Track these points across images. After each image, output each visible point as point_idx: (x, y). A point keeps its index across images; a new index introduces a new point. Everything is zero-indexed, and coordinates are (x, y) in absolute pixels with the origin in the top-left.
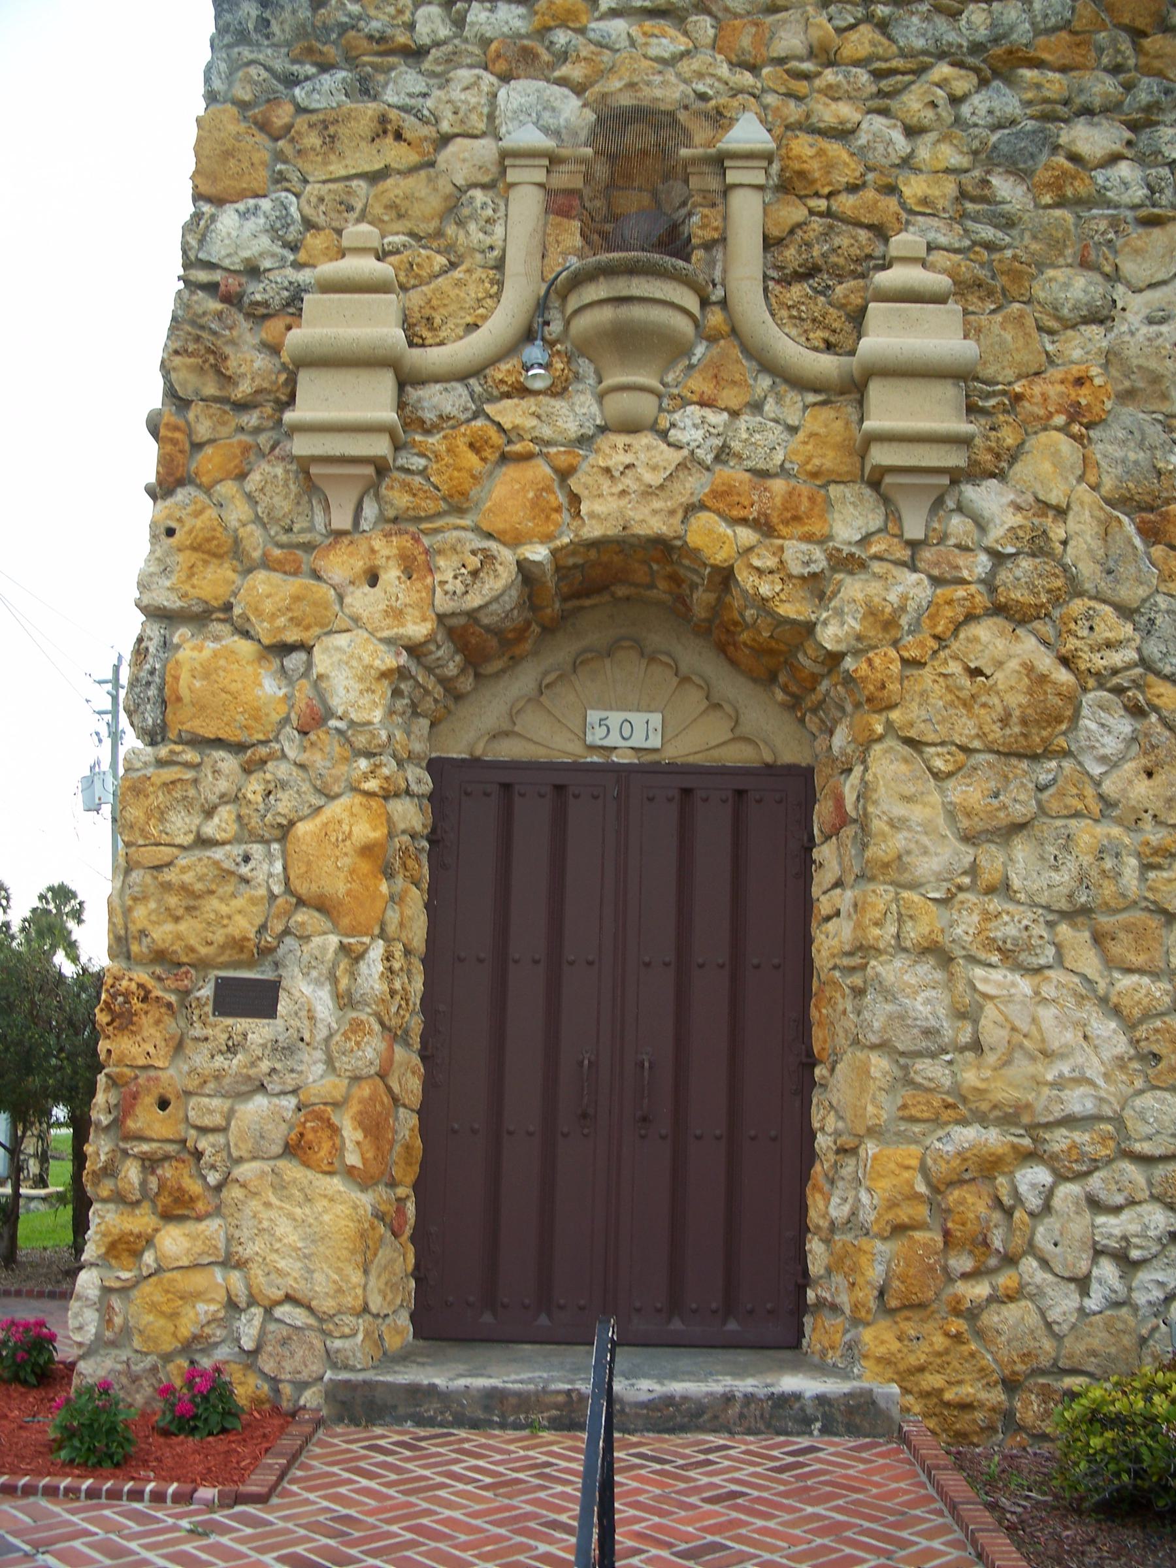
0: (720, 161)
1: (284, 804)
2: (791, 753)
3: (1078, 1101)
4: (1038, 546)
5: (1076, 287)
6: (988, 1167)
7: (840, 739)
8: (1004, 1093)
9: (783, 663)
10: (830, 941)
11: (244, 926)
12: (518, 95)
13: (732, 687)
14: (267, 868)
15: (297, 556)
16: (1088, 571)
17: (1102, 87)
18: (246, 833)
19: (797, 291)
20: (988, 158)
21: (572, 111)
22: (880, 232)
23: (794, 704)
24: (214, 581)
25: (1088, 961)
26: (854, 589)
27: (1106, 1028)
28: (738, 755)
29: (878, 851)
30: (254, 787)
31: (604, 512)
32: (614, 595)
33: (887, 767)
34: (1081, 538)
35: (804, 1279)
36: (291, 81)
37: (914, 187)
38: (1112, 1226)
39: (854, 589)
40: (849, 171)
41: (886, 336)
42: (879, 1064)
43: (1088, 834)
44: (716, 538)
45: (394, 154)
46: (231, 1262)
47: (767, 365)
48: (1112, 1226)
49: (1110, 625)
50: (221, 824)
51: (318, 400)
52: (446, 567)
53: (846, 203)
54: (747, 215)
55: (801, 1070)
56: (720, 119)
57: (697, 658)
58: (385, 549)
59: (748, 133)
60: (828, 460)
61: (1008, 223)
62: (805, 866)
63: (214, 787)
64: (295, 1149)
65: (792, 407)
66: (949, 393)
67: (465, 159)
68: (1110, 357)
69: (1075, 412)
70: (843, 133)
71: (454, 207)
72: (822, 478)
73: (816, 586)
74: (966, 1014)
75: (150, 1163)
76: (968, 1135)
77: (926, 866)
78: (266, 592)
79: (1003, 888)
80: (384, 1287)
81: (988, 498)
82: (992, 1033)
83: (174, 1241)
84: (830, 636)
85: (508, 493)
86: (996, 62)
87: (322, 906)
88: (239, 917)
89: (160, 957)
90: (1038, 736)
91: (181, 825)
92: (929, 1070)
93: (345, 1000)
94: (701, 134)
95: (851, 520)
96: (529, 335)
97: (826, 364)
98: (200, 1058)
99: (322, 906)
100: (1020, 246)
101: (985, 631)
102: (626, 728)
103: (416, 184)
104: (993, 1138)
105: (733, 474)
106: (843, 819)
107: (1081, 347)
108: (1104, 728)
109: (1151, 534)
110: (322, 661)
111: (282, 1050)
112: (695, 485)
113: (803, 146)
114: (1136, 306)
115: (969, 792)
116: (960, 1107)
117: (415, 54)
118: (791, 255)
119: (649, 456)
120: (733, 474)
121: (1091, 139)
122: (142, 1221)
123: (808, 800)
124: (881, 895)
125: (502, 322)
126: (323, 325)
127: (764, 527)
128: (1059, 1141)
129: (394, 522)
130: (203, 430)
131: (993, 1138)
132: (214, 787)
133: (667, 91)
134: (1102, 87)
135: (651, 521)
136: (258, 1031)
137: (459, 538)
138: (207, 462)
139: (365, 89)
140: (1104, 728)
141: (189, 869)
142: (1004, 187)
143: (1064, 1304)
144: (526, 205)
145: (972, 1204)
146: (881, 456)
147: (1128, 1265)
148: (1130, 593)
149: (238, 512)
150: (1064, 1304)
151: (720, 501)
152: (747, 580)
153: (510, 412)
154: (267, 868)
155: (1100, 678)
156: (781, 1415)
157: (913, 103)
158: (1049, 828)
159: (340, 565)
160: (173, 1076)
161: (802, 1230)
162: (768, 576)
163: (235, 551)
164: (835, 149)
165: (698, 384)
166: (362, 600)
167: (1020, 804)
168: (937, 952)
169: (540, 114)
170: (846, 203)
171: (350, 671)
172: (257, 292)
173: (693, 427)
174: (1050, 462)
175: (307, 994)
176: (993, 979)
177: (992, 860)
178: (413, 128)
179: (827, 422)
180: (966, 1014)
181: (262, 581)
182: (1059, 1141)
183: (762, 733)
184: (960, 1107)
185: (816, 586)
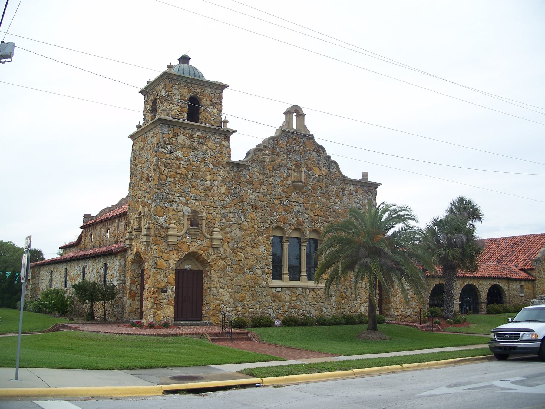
2: (201, 268)
3: (226, 299)
4: (225, 253)
5: (228, 230)
6: (219, 305)
9: (204, 262)
10: (206, 286)
11: (164, 285)
13: (197, 263)
14: (166, 280)
16: (228, 256)
17: (232, 210)
20: (222, 217)
21: (190, 210)
24: (161, 254)
25: (227, 288)
27: (228, 294)
28: (197, 269)
31: (192, 249)
32: (193, 256)
34: (228, 253)
35: (202, 314)
37: (217, 220)
39: (211, 257)
41: (215, 236)
42: (212, 296)
43: (227, 278)
44: (201, 252)
45: (174, 213)
54: (204, 222)
56: (202, 213)
58: (175, 252)
59: (204, 215)
60: (209, 245)
61: (224, 223)
64: (168, 304)
65: (206, 240)
66: (219, 241)
67: (181, 214)
70: (211, 214)
71: (179, 219)
73: (208, 257)
74: (218, 292)
75: (156, 306)
77: (215, 280)
78: (165, 255)
81: (221, 249)
82: (220, 294)
83: (159, 312)
84: (209, 261)
85: (185, 247)
86: (223, 207)
90: (224, 270)
91: (159, 276)
92: (215, 297)
93: (172, 291)
94: (200, 214)
95: (211, 251)
96: (186, 232)
97: (209, 237)
101: (220, 261)
102: (189, 267)
103: (176, 216)
105: (202, 246)
106: (207, 276)
108: (229, 269)
110: (170, 262)
111: (167, 296)
112: (199, 247)
114: (233, 231)
115: (218, 274)
116: (217, 300)
119: (195, 244)
120: (202, 246)
121: (231, 215)
125: (184, 231)
127: (204, 251)
128: (225, 302)
129: (175, 250)
130: (158, 239)
133: (198, 209)
134: (232, 210)
136: (166, 294)
139: (171, 205)
140: (229, 269)
141: (160, 280)
145: (218, 307)
146: (214, 246)
147: (229, 312)
148: (231, 258)
149: (162, 248)
151: (200, 249)
153: (184, 240)
154: (166, 280)
160: (158, 298)
162: (204, 255)
166: (173, 257)
168: (216, 287)
169: (187, 210)
171: (172, 263)
173: (199, 242)
174: (226, 246)
175: (169, 291)
176: (220, 290)
177: (220, 280)
178: (176, 211)
179: (209, 242)
180: (218, 292)
182: (225, 302)
183: (199, 267)
184: (217, 300)
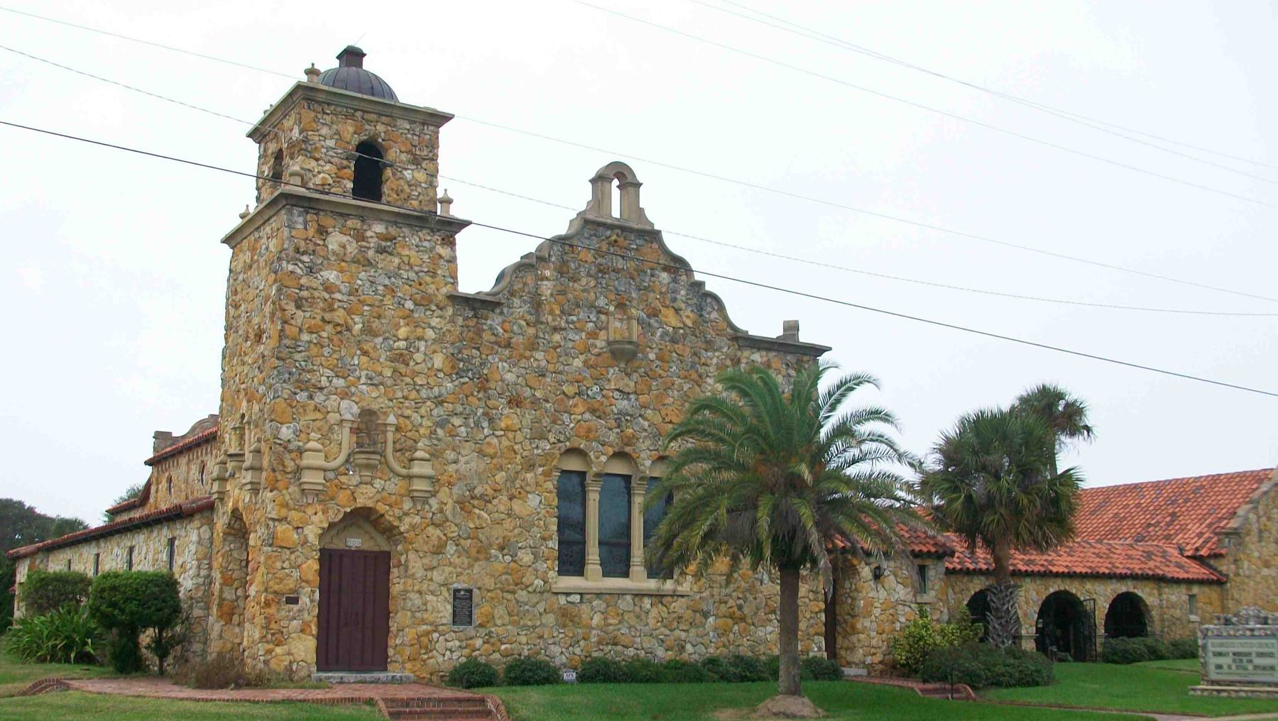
0: (386, 425)
1: (299, 561)
2: (386, 549)
4: (441, 511)
5: (451, 455)
6: (428, 633)
7: (400, 548)
8: (431, 619)
9: (390, 532)
10: (395, 589)
11: (292, 586)
12: (345, 404)
13: (374, 533)
14: (296, 574)
15: (301, 508)
16: (450, 517)
18: (292, 567)
19: (398, 454)
21: (356, 409)
22: (416, 442)
23: (388, 538)
24: (284, 512)
26: (407, 520)
28: (376, 549)
29: (410, 572)
30: (293, 557)
31: (361, 502)
32: (362, 517)
33: (412, 555)
35: (387, 657)
36: (296, 394)
37: (422, 431)
38: (449, 644)
40: (410, 427)
43: (447, 569)
44: (382, 508)
45: (319, 416)
46: (289, 654)
47: (392, 471)
48: (449, 644)
49: (454, 528)
50: (286, 565)
51: (308, 477)
52: (331, 512)
53: (409, 434)
55: (387, 615)
57: (371, 529)
58: (319, 508)
59: (392, 419)
60: (403, 492)
61: (439, 440)
62: (388, 572)
63: (284, 557)
64: (302, 631)
65: (395, 480)
66: (427, 481)
67: (333, 418)
68: (457, 471)
69: (449, 483)
70: (408, 417)
72: (402, 496)
73: (400, 519)
74: (425, 604)
75: (273, 634)
76: (424, 627)
77: (418, 575)
79: (431, 580)
80: (312, 657)
81: (433, 502)
82: (429, 608)
83: (278, 650)
87: (307, 582)
88: (291, 584)
89: (275, 592)
90: (439, 550)
91: (279, 565)
93: (312, 601)
94: (382, 417)
97: (404, 472)
98: (283, 613)
99: (307, 582)
100: (442, 445)
101: (430, 528)
102: (355, 542)
104: (429, 628)
107: (452, 468)
108: (451, 548)
109: (462, 509)
110: (306, 531)
113: (401, 420)
114: (462, 460)
115: (425, 561)
116: (423, 621)
117: (321, 389)
118: (398, 446)
120: (385, 494)
122: (271, 646)
123: (389, 558)
124: (410, 581)
126: (308, 460)
127: (390, 506)
128: (441, 628)
129: (320, 502)
131: (429, 628)
132: (284, 557)
135: (370, 504)
136: (296, 607)
137: (331, 505)
138: (280, 485)
141: (280, 574)
142: (439, 431)
143: (440, 659)
144: (346, 431)
145: (425, 640)
146: (416, 494)
148: (457, 521)
149: (287, 497)
150: (440, 659)
151: (383, 500)
152: (387, 517)
154: (296, 574)
155: (451, 539)
156: (377, 681)
157: (423, 411)
158: (440, 568)
159: (310, 511)
160: (277, 617)
161: (387, 647)
163: (286, 506)
164: (408, 422)
165: (379, 474)
167: (435, 563)
168: (420, 592)
170: (409, 434)
171: (312, 533)
172: (291, 447)
174: (444, 494)
175: (304, 600)
176: (429, 597)
177: (429, 574)
181: (293, 513)
182: (441, 628)
183: (381, 544)
184: (423, 621)
185: (400, 519)
